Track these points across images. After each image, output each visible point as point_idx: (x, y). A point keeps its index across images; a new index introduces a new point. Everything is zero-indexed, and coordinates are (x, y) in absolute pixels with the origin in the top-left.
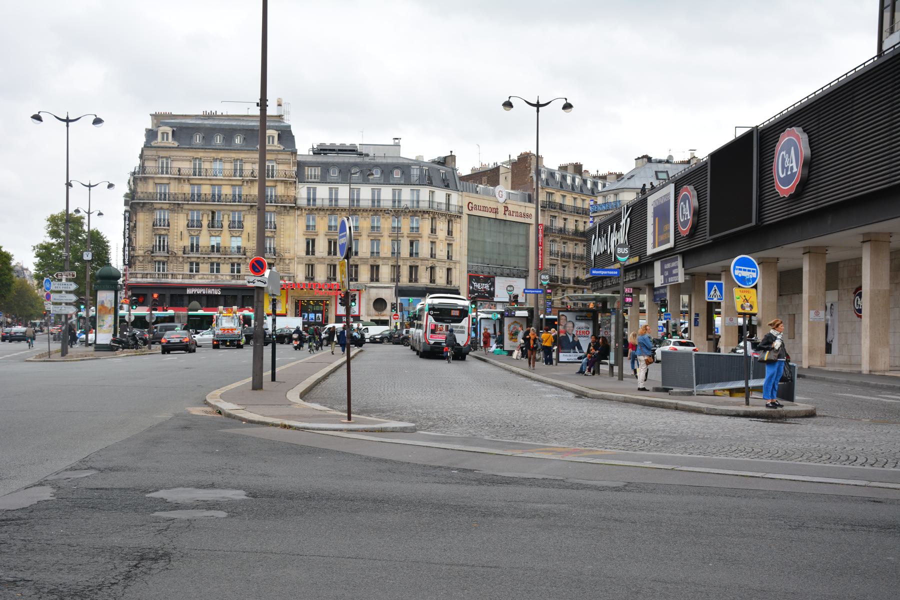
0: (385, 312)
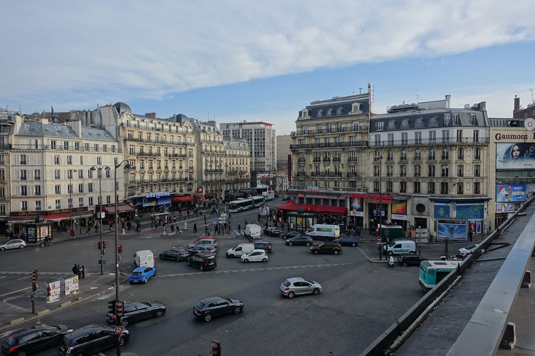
0: (424, 213)
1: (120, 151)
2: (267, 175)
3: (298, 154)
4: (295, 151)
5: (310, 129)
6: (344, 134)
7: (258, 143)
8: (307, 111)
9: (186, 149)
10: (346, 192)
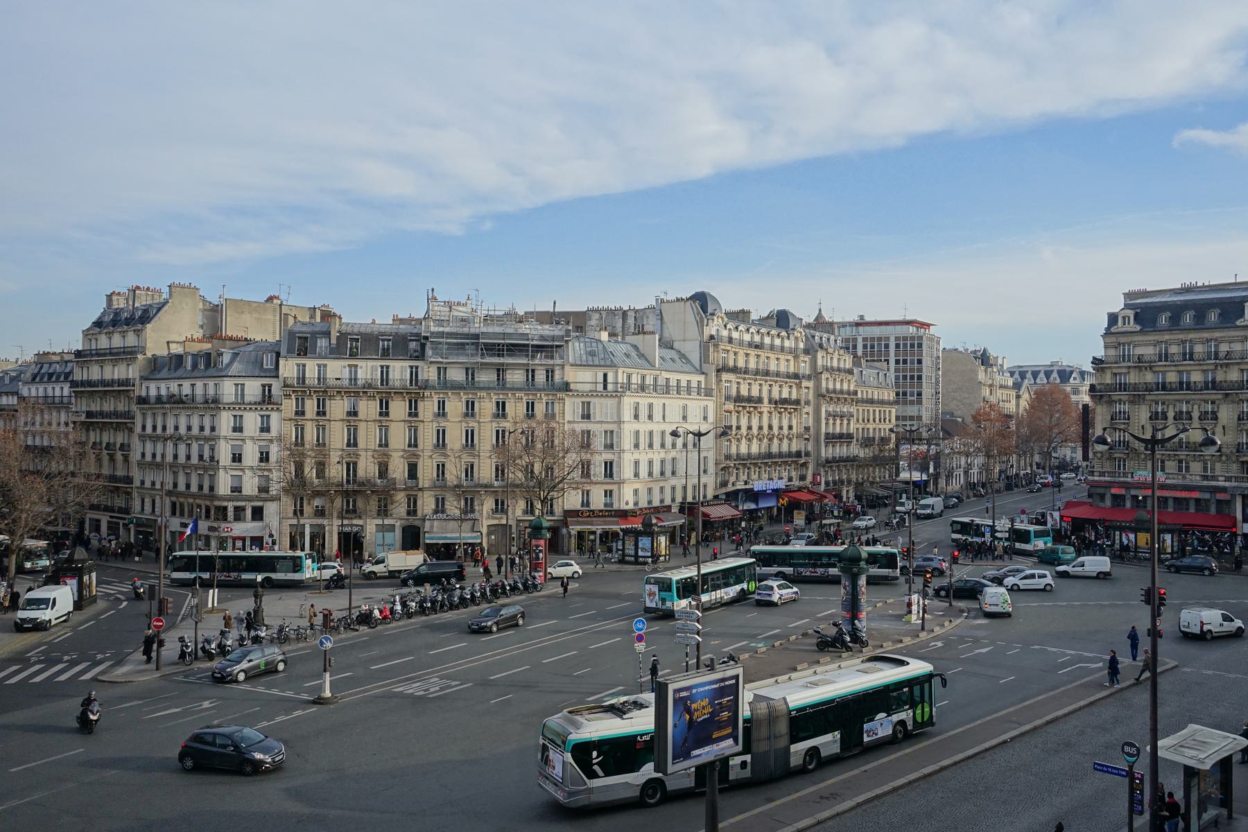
1: (709, 393)
2: (924, 448)
3: (1111, 402)
4: (1101, 396)
5: (1139, 351)
6: (1227, 365)
7: (904, 370)
8: (1131, 313)
9: (799, 386)
10: (1234, 484)
